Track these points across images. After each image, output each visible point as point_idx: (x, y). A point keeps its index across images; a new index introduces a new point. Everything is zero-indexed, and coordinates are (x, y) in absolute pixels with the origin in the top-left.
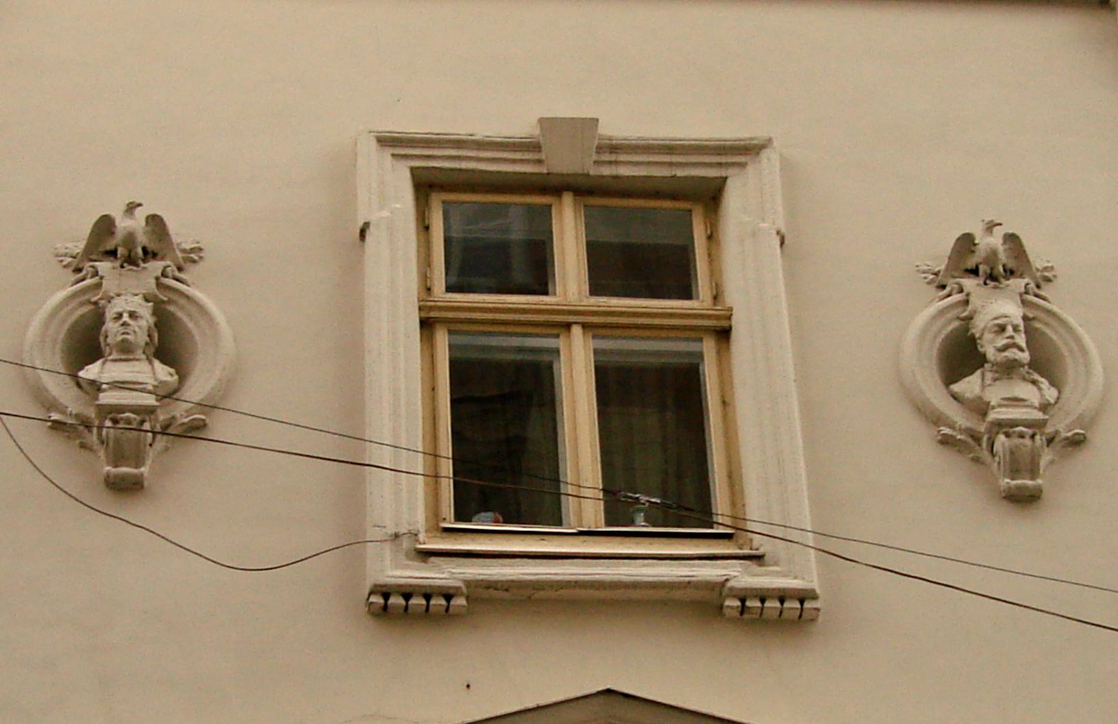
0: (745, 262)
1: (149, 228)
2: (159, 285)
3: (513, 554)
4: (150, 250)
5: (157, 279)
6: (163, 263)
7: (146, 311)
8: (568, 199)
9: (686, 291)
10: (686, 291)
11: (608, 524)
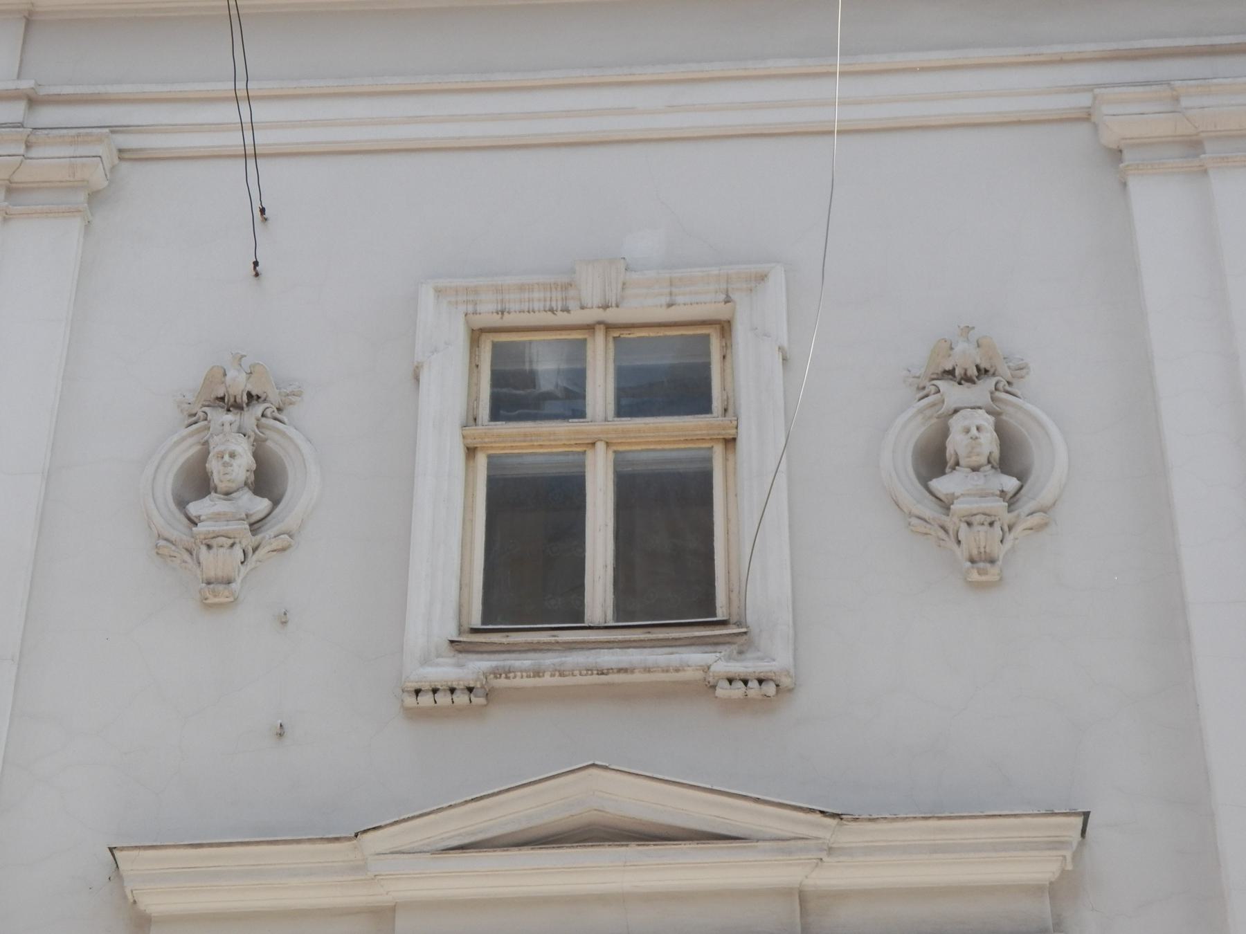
0: (750, 378)
1: (527, 367)
2: (993, 399)
3: (541, 658)
4: (254, 393)
5: (992, 393)
6: (994, 380)
7: (987, 421)
8: (600, 336)
9: (706, 408)
10: (706, 408)
11: (617, 621)
